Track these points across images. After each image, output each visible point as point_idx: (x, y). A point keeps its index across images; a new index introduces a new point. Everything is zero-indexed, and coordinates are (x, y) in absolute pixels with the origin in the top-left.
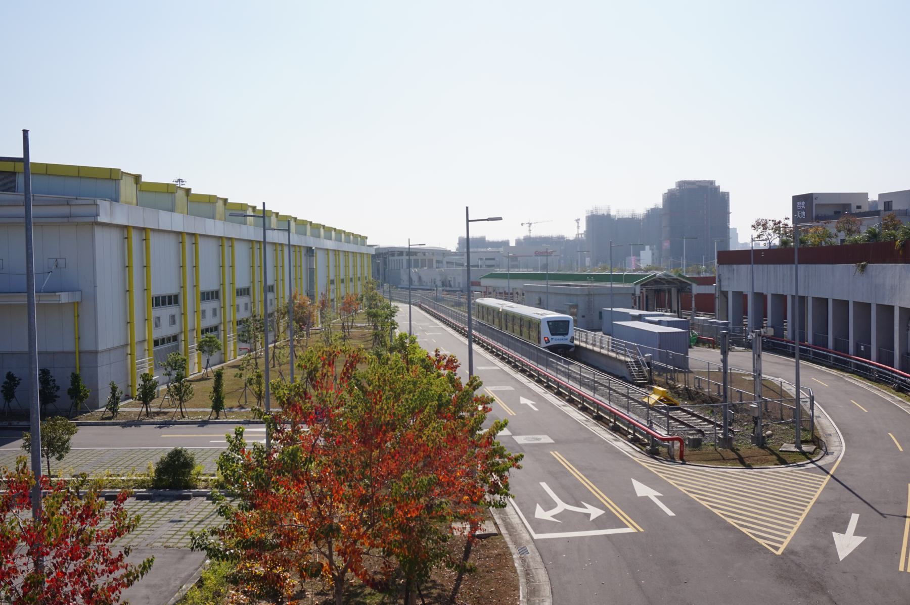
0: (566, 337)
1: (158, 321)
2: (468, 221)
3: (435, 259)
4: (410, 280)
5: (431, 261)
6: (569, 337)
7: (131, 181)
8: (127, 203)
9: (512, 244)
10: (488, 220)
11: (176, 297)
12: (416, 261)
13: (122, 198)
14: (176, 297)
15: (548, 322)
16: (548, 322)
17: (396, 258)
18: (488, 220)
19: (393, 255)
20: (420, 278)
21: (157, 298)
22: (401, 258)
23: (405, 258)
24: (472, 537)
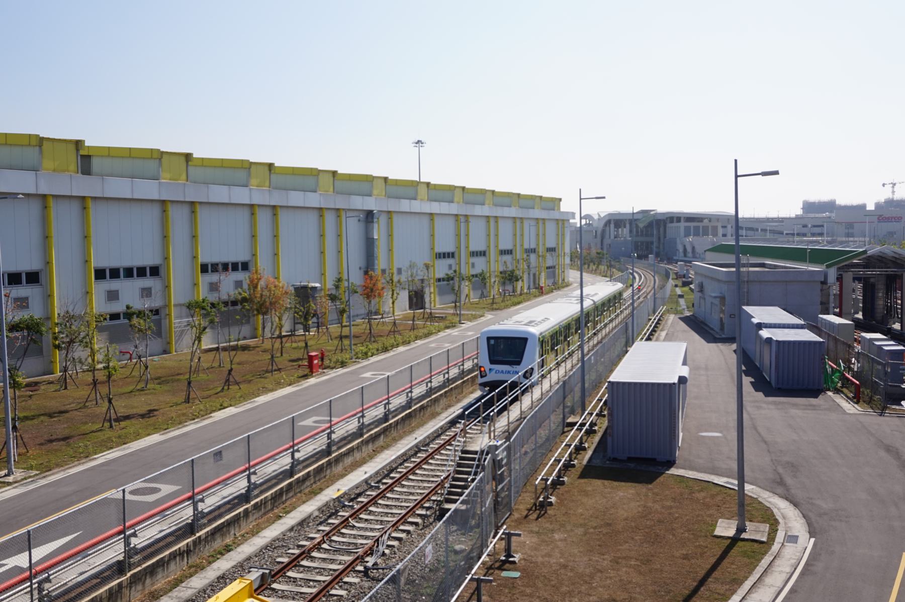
0: (516, 368)
1: (473, 265)
2: (737, 176)
3: (719, 225)
4: (685, 251)
5: (715, 229)
6: (522, 370)
7: (425, 186)
8: (421, 200)
9: (596, 217)
10: (765, 174)
11: (453, 254)
12: (697, 229)
13: (419, 197)
14: (453, 254)
15: (489, 339)
16: (489, 339)
17: (675, 224)
18: (765, 174)
19: (672, 222)
20: (693, 248)
21: (440, 254)
22: (678, 224)
23: (683, 224)
24: (735, 540)
